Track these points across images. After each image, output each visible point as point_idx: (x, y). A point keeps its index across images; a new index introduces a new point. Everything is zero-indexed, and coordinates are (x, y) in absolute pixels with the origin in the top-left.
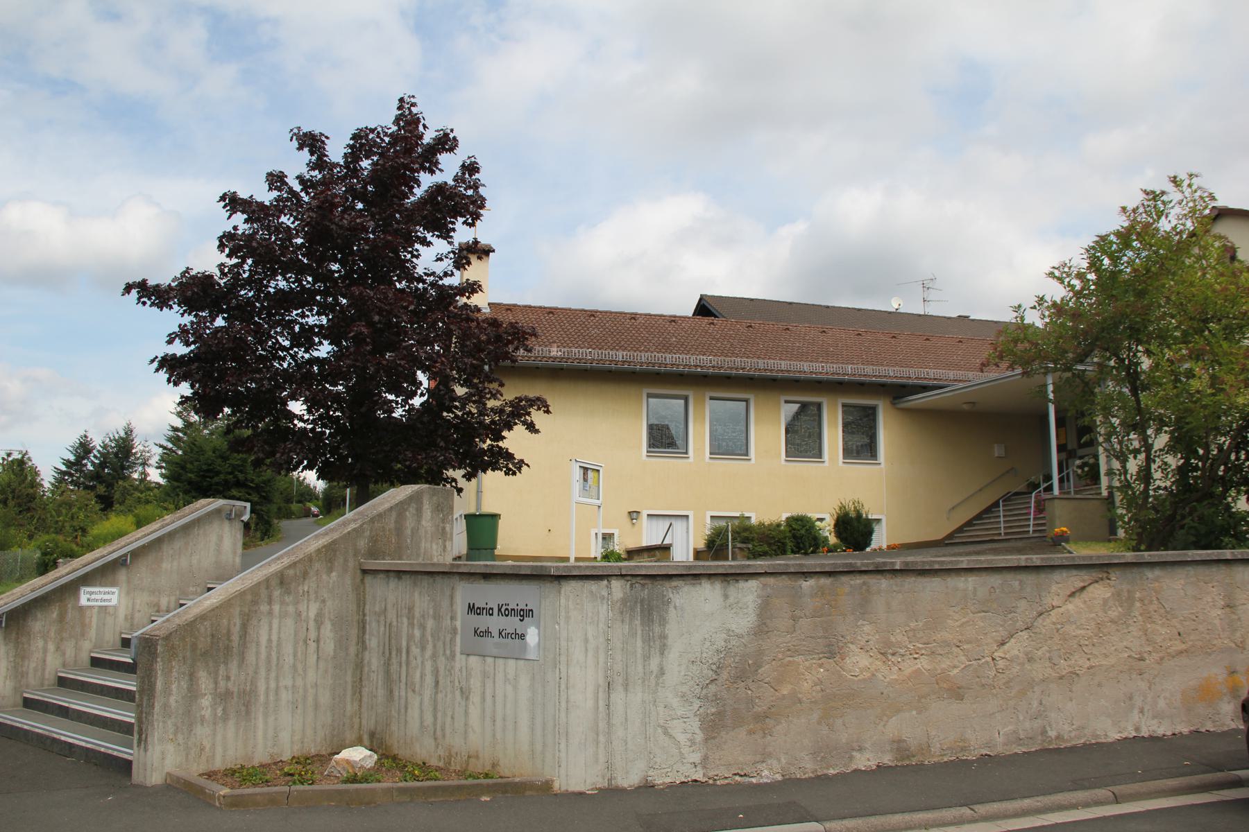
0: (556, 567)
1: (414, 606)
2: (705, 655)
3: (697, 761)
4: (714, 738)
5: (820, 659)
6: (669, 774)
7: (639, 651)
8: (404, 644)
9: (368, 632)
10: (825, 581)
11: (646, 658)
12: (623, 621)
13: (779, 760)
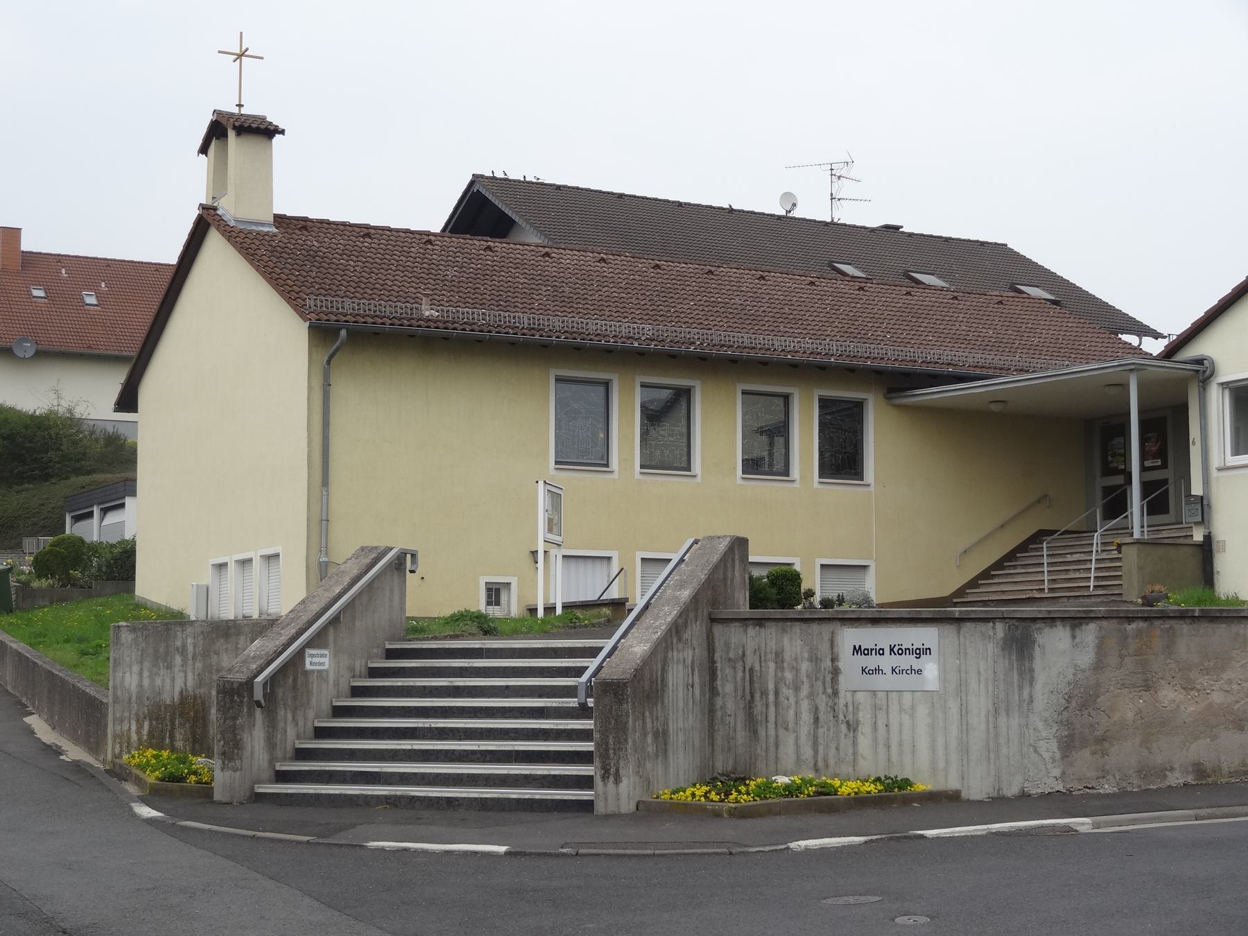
0: (959, 611)
1: (783, 651)
2: (1060, 686)
3: (1058, 776)
4: (1067, 757)
5: (1140, 691)
6: (1039, 786)
7: (1016, 682)
8: (771, 686)
9: (719, 677)
10: (1142, 624)
11: (1021, 688)
12: (1004, 657)
13: (1115, 777)
